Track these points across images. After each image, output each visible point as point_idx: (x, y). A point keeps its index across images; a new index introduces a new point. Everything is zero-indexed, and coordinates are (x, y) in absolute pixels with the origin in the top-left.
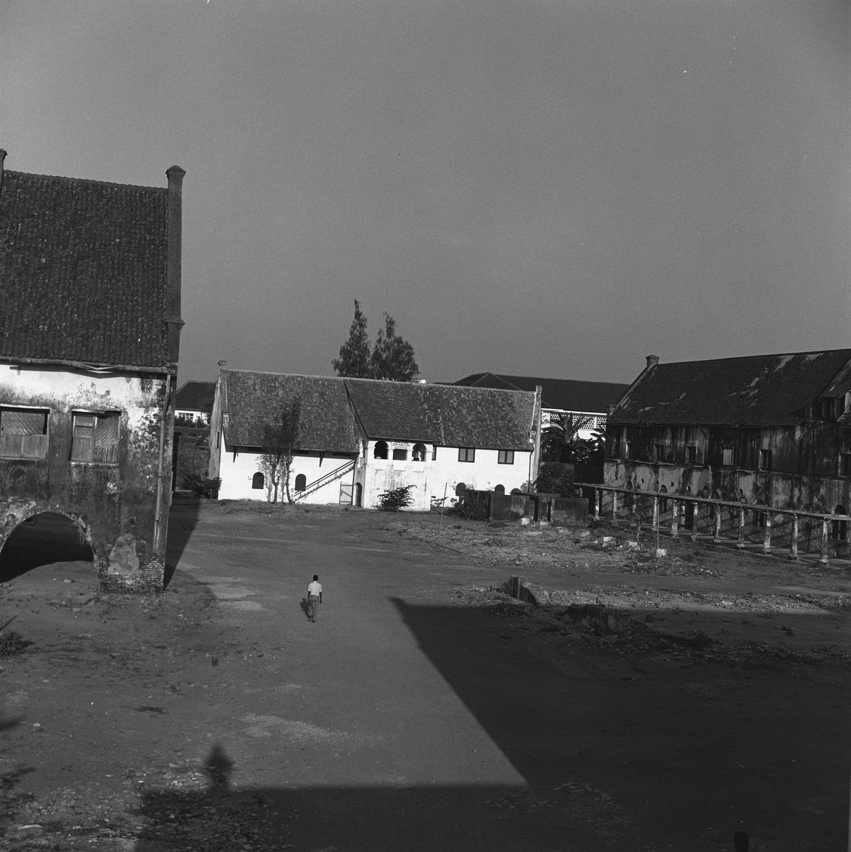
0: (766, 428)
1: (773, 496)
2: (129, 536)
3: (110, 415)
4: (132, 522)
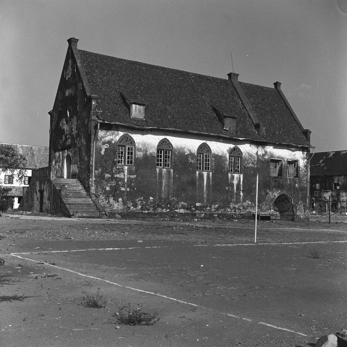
0: (336, 176)
1: (341, 198)
2: (301, 201)
3: (294, 162)
4: (302, 197)
